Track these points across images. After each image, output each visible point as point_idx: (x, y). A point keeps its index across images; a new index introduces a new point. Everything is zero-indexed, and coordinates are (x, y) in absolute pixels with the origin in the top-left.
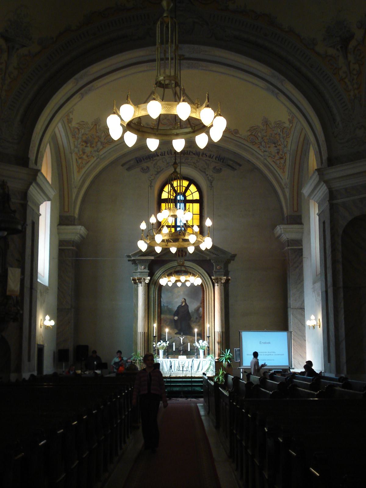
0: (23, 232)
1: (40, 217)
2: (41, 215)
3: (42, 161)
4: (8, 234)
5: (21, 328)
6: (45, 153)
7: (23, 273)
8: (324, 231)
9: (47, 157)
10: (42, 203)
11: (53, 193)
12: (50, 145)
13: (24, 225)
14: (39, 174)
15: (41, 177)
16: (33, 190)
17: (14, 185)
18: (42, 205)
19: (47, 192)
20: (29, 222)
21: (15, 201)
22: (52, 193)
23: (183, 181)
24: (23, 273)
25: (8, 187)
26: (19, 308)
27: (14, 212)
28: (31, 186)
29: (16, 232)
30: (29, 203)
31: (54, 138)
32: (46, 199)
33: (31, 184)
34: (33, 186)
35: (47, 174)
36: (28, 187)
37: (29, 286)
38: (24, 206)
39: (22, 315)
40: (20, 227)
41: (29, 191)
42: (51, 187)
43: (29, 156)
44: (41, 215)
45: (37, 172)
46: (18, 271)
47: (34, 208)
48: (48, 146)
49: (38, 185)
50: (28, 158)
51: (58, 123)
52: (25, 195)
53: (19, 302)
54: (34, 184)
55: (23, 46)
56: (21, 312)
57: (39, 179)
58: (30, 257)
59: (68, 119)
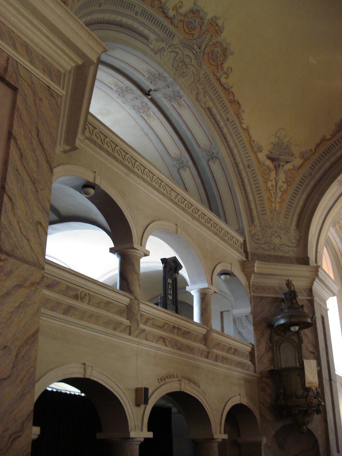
0: (312, 325)
1: (329, 312)
2: (328, 310)
3: (322, 260)
4: (299, 329)
5: (326, 421)
6: (324, 255)
7: (319, 364)
8: (325, 334)
9: (325, 256)
10: (327, 299)
11: (337, 289)
12: (326, 248)
13: (313, 317)
14: (320, 270)
15: (323, 273)
16: (317, 286)
17: (299, 284)
18: (328, 300)
19: (332, 289)
20: (318, 315)
21: (302, 298)
22: (335, 288)
23: (294, 365)
24: (319, 364)
25: (293, 285)
26: (320, 400)
27: (302, 306)
28: (315, 282)
29: (308, 325)
30: (316, 299)
31: (329, 243)
32: (331, 295)
33: (314, 280)
34: (317, 282)
35: (329, 272)
36: (312, 284)
37: (328, 378)
38: (311, 302)
39: (324, 407)
40: (309, 320)
41: (313, 287)
42: (334, 282)
43: (309, 256)
44: (328, 310)
45: (317, 269)
46: (314, 362)
47: (321, 303)
48: (325, 248)
49: (321, 280)
50: (308, 258)
51: (329, 227)
52: (310, 291)
53: (320, 394)
54: (317, 280)
55: (288, 162)
56: (323, 403)
57: (321, 274)
58: (325, 350)
59: (340, 226)
